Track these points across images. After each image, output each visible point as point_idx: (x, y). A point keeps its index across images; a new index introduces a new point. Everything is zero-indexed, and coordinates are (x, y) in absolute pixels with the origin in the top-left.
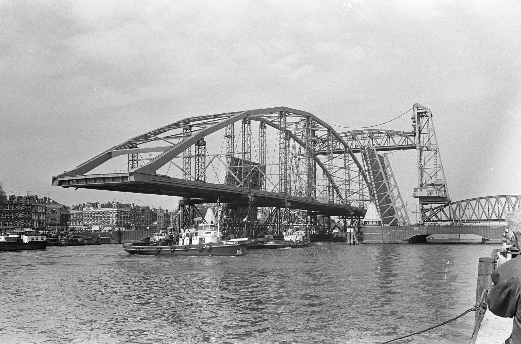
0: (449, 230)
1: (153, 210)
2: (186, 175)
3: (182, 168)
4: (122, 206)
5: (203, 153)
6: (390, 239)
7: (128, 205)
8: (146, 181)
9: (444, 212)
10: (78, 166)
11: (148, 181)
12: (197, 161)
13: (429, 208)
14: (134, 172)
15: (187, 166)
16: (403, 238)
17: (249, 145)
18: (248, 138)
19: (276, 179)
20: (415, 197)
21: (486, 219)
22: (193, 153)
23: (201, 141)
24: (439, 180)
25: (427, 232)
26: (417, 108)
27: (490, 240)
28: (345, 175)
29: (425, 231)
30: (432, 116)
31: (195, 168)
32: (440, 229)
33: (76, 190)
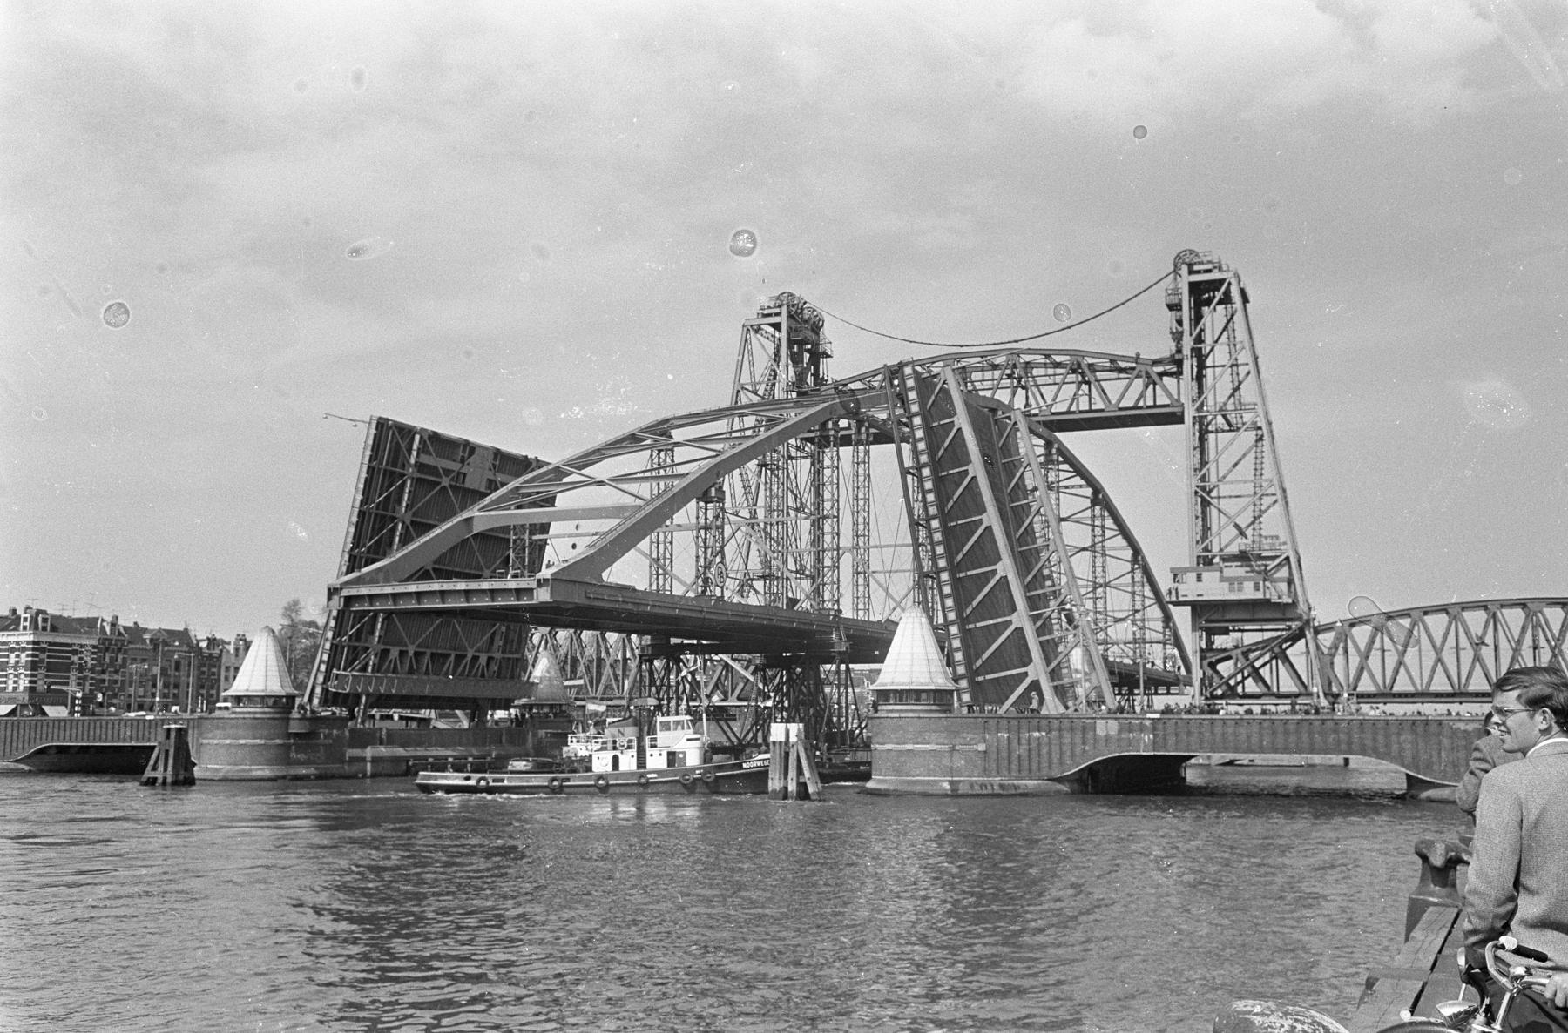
0: (1255, 737)
1: (204, 645)
4: (56, 624)
6: (986, 772)
7: (90, 624)
8: (580, 602)
9: (1286, 660)
12: (702, 544)
13: (1230, 646)
14: (549, 577)
15: (661, 550)
16: (1050, 767)
17: (836, 496)
18: (832, 476)
21: (1449, 689)
23: (713, 490)
25: (1154, 743)
26: (1190, 265)
28: (1094, 572)
29: (1147, 738)
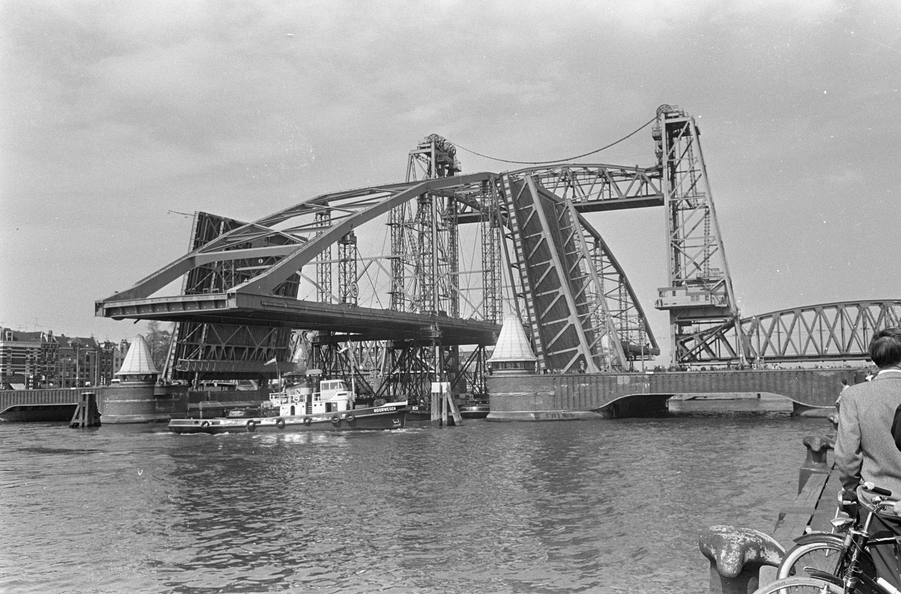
1: (103, 346)
2: (322, 292)
3: (316, 282)
5: (353, 257)
6: (555, 407)
9: (724, 339)
10: (139, 283)
11: (260, 307)
13: (692, 332)
15: (324, 278)
19: (477, 297)
20: (661, 309)
22: (335, 256)
23: (348, 236)
24: (714, 272)
26: (666, 114)
27: (815, 408)
29: (647, 385)
30: (698, 133)
31: (340, 282)
32: (683, 382)
33: (135, 323)
